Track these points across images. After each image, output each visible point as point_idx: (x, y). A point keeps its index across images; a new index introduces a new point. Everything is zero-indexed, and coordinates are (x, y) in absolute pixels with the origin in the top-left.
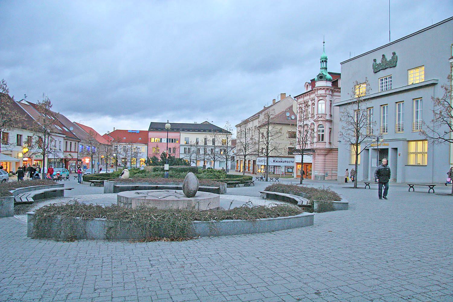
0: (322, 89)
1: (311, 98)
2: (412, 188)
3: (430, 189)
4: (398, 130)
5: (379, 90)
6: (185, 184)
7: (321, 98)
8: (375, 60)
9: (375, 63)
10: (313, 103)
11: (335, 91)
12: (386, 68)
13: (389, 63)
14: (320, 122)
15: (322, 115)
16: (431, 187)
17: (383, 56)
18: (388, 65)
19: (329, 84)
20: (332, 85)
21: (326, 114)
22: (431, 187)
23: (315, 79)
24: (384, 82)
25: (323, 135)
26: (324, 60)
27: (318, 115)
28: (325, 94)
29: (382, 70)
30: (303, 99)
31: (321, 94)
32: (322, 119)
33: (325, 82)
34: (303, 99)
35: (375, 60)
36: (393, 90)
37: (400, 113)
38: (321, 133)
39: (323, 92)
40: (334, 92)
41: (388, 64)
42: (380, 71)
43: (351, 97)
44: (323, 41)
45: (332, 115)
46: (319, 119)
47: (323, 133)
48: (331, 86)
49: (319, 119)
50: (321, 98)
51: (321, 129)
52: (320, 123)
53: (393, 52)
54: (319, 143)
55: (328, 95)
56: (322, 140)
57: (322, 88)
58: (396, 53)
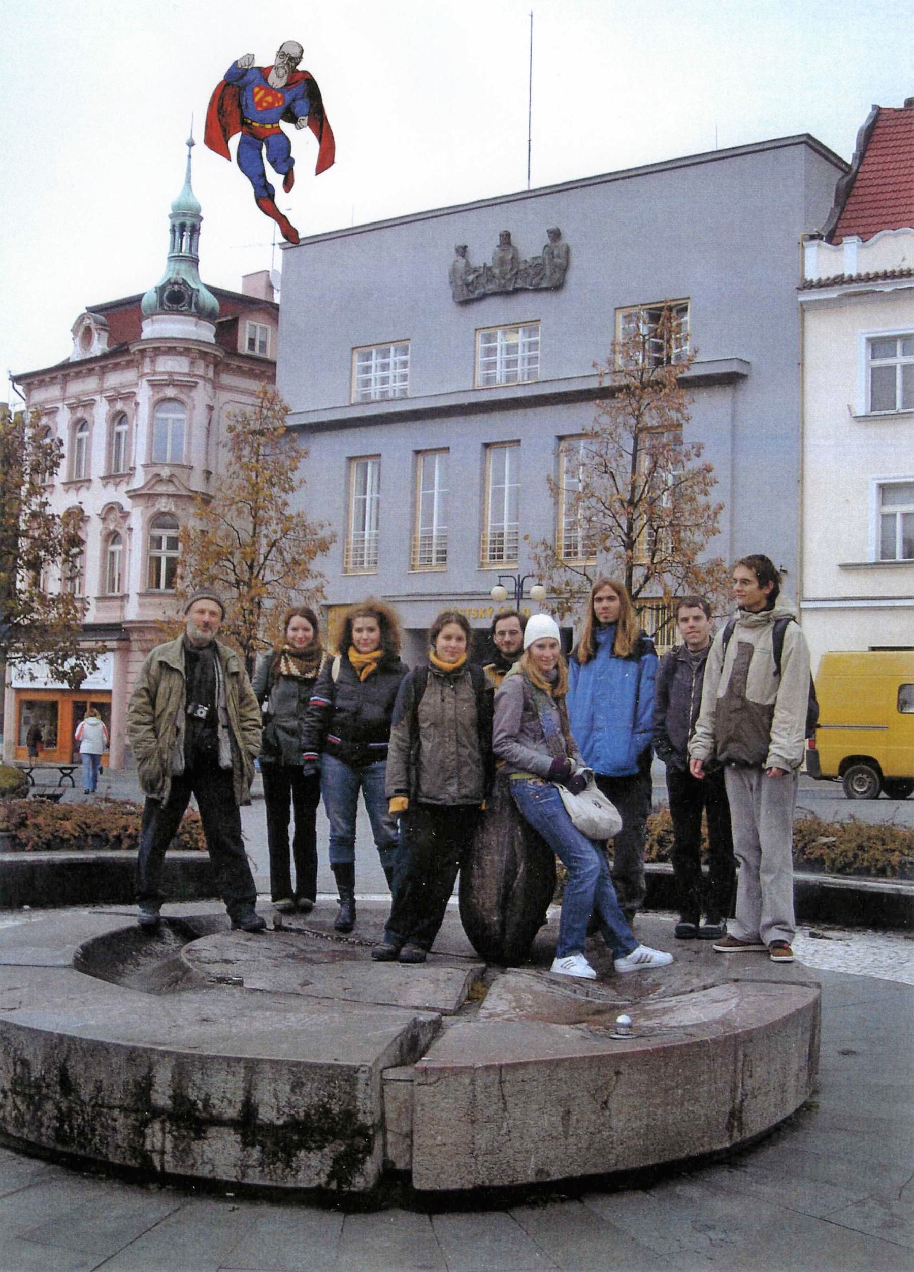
0: (180, 354)
1: (69, 398)
2: (67, 778)
3: (62, 778)
4: (438, 559)
5: (354, 395)
6: (516, 865)
7: (170, 392)
8: (463, 251)
9: (462, 261)
10: (120, 412)
11: (228, 368)
12: (516, 291)
13: (531, 271)
14: (163, 500)
15: (177, 471)
16: (68, 771)
17: (506, 238)
18: (528, 280)
19: (206, 332)
20: (216, 336)
21: (192, 468)
22: (64, 771)
23: (144, 301)
24: (395, 363)
25: (171, 561)
26: (189, 222)
27: (156, 470)
28: (188, 375)
29: (494, 294)
30: (64, 389)
31: (170, 374)
32: (171, 489)
33: (194, 319)
34: (64, 389)
35: (463, 251)
36: (701, 366)
37: (433, 494)
38: (164, 553)
39: (180, 366)
40: (223, 371)
41: (528, 274)
42: (483, 297)
43: (594, 365)
44: (188, 137)
45: (211, 473)
46: (161, 489)
47: (173, 554)
48: (213, 341)
49: (161, 489)
50: (170, 392)
51: (166, 534)
52: (163, 505)
53: (552, 227)
54: (157, 600)
55: (201, 383)
56: (170, 584)
57: (180, 346)
58: (564, 230)
